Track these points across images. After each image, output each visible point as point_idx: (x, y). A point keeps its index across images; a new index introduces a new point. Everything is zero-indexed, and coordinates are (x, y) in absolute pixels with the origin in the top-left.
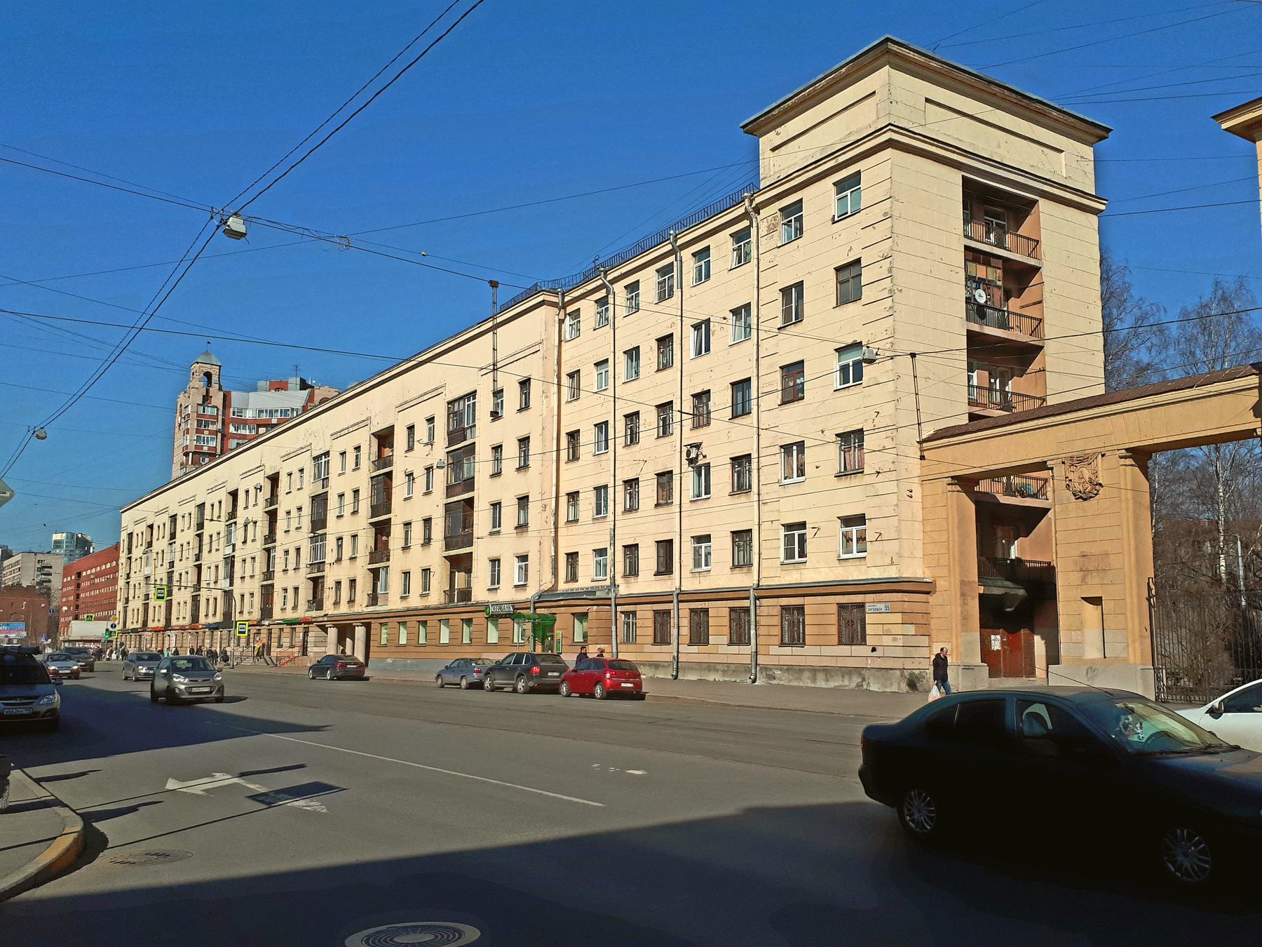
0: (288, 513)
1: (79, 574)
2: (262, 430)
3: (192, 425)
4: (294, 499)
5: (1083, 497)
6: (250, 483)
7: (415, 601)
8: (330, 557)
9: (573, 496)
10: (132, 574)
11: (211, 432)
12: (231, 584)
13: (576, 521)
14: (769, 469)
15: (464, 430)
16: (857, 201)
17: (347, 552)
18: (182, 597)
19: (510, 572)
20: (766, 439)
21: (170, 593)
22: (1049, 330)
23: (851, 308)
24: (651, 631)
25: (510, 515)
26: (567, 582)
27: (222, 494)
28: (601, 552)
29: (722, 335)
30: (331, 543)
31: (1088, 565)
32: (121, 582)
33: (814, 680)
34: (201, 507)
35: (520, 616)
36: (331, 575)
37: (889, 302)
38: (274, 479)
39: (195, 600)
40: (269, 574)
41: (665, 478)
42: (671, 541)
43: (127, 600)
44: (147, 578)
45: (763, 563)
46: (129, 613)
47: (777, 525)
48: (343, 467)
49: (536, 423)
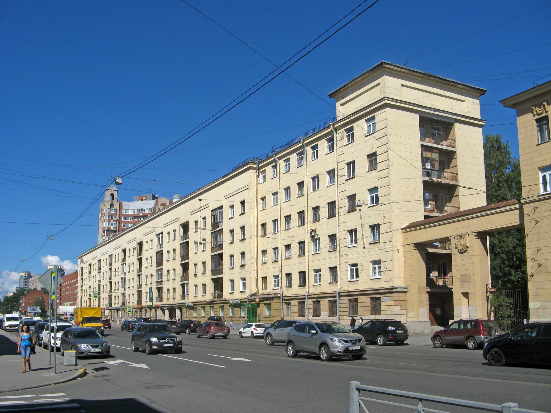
3: (106, 218)
4: (149, 253)
6: (131, 246)
7: (200, 299)
8: (164, 279)
9: (264, 252)
11: (114, 221)
12: (125, 290)
13: (265, 263)
14: (344, 239)
15: (218, 223)
16: (374, 128)
17: (171, 277)
18: (104, 296)
20: (342, 227)
21: (99, 294)
24: (297, 311)
26: (263, 290)
27: (120, 251)
28: (276, 277)
29: (325, 180)
30: (165, 272)
32: (79, 289)
34: (111, 256)
36: (165, 286)
38: (140, 244)
39: (110, 296)
40: (140, 286)
41: (302, 244)
43: (82, 297)
44: (90, 287)
45: (342, 281)
46: (83, 302)
48: (169, 239)
49: (251, 220)
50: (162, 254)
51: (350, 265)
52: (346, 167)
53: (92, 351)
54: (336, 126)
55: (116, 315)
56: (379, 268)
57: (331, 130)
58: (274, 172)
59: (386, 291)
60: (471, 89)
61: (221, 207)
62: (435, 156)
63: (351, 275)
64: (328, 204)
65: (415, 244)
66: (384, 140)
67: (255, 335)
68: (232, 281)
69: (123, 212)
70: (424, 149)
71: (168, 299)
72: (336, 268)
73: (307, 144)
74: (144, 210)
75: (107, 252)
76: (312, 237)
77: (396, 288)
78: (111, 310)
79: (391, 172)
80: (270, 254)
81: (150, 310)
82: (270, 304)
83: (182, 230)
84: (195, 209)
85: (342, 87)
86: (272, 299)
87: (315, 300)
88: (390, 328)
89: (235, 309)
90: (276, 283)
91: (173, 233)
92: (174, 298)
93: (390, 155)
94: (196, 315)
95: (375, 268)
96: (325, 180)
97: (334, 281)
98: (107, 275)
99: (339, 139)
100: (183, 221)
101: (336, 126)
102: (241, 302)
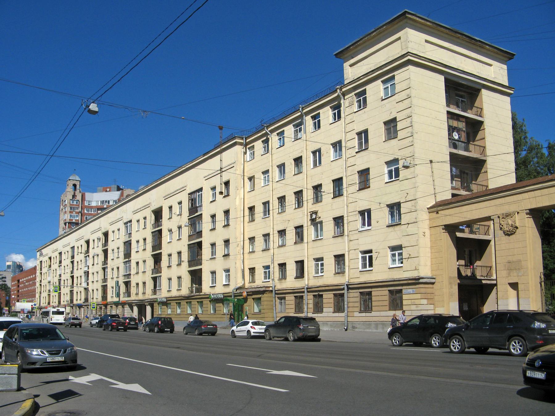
0: (113, 250)
1: (19, 281)
2: (99, 212)
3: (68, 209)
4: (116, 243)
5: (508, 234)
8: (133, 272)
9: (252, 239)
10: (42, 280)
11: (76, 213)
12: (88, 285)
14: (353, 223)
15: (197, 207)
18: (65, 291)
19: (221, 278)
21: (60, 289)
22: (489, 152)
23: (393, 142)
25: (220, 249)
26: (250, 283)
28: (268, 267)
29: (329, 154)
31: (513, 266)
32: (38, 284)
33: (377, 329)
34: (73, 248)
35: (227, 300)
36: (134, 280)
37: (411, 139)
38: (106, 234)
39: (72, 292)
40: (105, 280)
41: (299, 230)
42: (303, 261)
43: (41, 293)
44: (49, 282)
46: (42, 298)
47: (358, 251)
49: (238, 201)
50: (131, 244)
51: (361, 252)
52: (356, 137)
53: (49, 360)
54: (343, 90)
55: (78, 312)
56: (400, 254)
57: (338, 96)
58: (265, 147)
59: (410, 282)
60: (499, 52)
61: (201, 189)
62: (461, 125)
63: (362, 264)
64: (333, 181)
65: (445, 225)
66: (406, 103)
67: (252, 334)
68: (213, 273)
69: (86, 204)
70: (450, 116)
71: (137, 294)
72: (343, 255)
73: (307, 114)
74: (109, 201)
75: (69, 244)
76: (313, 221)
77: (423, 278)
78: (72, 307)
79: (415, 141)
80: (260, 243)
81: (117, 306)
82: (260, 299)
83: (153, 217)
84: (169, 193)
85: (352, 45)
86: (263, 292)
87: (317, 293)
88: (537, 325)
89: (217, 305)
90: (267, 275)
91: (144, 221)
92: (144, 293)
93: (413, 120)
94: (169, 311)
95: (394, 255)
96: (329, 154)
97: (340, 271)
98: (69, 270)
99: (347, 104)
100: (155, 206)
101: (343, 90)
102: (224, 296)
